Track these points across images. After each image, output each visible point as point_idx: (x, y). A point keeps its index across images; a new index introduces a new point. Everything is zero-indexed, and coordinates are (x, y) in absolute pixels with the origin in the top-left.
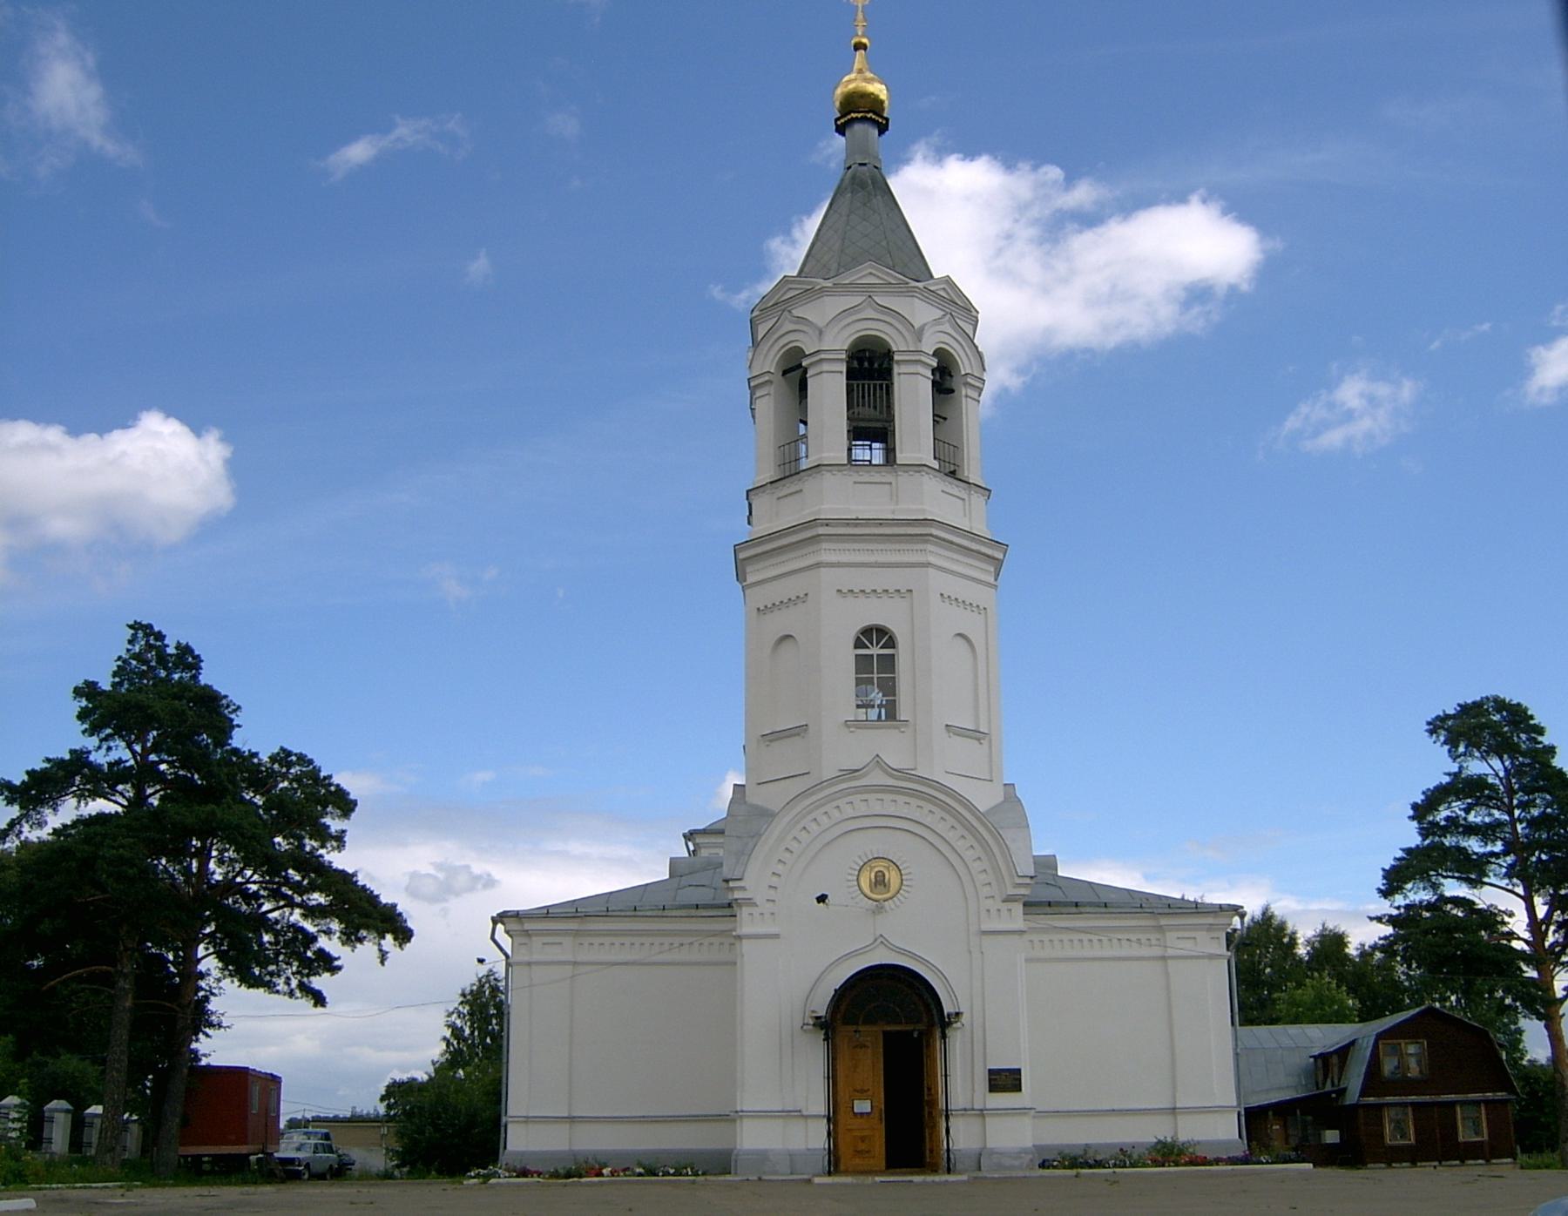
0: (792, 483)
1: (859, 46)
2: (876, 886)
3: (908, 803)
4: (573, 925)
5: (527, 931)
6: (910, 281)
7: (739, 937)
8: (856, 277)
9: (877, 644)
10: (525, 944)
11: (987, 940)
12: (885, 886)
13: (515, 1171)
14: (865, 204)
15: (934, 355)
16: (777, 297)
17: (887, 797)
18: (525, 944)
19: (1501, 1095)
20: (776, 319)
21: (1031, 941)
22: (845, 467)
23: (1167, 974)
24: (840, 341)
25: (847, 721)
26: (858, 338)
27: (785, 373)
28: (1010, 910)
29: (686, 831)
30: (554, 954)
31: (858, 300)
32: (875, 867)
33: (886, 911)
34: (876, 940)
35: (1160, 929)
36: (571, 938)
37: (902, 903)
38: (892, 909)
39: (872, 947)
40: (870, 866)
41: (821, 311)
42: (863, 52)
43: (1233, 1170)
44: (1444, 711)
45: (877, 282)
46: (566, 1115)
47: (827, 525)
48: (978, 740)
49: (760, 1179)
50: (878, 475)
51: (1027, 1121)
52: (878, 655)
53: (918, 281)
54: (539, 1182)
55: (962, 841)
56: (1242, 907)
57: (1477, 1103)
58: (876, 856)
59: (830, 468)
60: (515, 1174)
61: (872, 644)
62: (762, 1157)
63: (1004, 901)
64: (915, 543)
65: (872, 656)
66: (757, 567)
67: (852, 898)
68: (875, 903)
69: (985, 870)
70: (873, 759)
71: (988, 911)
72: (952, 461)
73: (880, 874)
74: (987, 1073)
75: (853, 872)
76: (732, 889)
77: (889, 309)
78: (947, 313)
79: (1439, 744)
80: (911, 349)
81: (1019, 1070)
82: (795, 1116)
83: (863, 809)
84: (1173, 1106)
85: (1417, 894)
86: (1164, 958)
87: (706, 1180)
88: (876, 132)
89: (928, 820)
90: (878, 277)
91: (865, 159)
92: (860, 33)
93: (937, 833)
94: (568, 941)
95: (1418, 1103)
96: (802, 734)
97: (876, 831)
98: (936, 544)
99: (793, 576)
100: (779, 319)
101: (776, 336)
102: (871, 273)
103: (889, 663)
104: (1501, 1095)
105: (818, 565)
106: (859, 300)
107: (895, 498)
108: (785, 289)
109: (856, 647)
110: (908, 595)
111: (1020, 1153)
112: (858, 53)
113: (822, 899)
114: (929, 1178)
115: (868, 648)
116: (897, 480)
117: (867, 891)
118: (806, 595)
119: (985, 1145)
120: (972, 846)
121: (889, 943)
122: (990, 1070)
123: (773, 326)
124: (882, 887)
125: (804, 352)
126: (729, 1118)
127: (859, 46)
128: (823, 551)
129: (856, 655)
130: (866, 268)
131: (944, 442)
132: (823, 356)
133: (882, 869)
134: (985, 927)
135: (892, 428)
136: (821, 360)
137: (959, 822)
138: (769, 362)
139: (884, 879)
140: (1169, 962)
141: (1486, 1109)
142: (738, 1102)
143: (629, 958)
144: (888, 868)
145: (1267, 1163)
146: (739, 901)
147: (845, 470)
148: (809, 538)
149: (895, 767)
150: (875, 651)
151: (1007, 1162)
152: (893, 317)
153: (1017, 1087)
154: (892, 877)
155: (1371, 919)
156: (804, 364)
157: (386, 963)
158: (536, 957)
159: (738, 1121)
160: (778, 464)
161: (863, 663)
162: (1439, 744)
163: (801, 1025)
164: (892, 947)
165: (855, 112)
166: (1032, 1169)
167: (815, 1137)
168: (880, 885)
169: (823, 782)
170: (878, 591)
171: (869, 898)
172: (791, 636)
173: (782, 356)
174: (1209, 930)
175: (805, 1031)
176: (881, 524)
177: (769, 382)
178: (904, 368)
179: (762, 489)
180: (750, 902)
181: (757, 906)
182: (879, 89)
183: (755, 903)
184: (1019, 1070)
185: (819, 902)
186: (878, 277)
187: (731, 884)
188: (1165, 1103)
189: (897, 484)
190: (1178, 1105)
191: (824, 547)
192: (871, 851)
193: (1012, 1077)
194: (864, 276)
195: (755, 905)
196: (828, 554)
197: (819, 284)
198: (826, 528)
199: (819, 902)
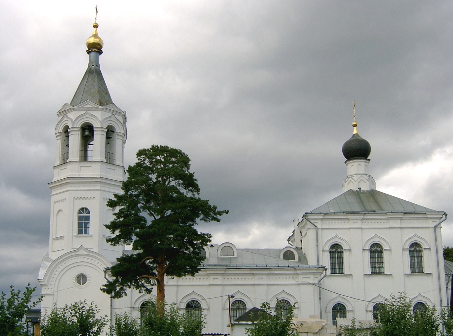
9: (85, 213)
15: (107, 128)
26: (83, 123)
41: (73, 115)
52: (85, 216)
61: (83, 213)
65: (83, 216)
72: (110, 158)
75: (74, 280)
76: (40, 282)
102: (88, 104)
103: (88, 218)
106: (84, 112)
109: (79, 213)
115: (82, 214)
118: (94, 197)
129: (79, 216)
131: (109, 153)
138: (61, 130)
148: (109, 184)
150: (84, 215)
156: (68, 131)
161: (80, 218)
172: (61, 210)
174: (267, 275)
187: (40, 281)
192: (75, 274)
194: (86, 105)
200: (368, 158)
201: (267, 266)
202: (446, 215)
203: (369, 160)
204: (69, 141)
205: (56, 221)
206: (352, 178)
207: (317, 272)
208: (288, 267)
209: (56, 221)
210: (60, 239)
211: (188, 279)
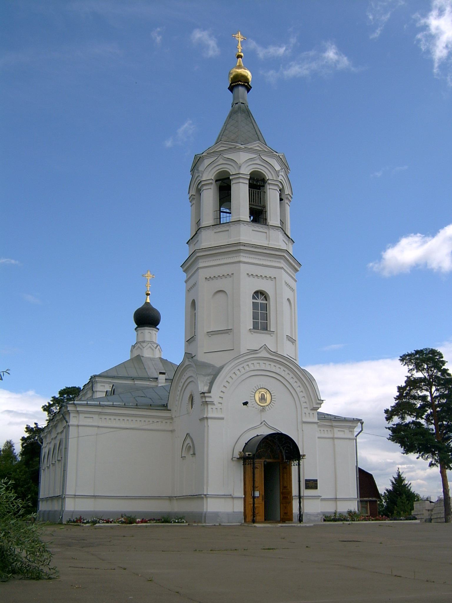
0: (223, 227)
1: (239, 56)
2: (261, 400)
3: (275, 366)
4: (99, 410)
5: (78, 411)
6: (274, 152)
7: (207, 418)
8: (254, 146)
10: (76, 417)
11: (305, 426)
12: (265, 400)
13: (105, 520)
14: (246, 119)
16: (216, 149)
17: (267, 363)
18: (76, 417)
19: (374, 499)
20: (217, 157)
22: (250, 223)
23: (334, 445)
24: (246, 171)
25: (250, 329)
27: (216, 181)
28: (313, 414)
29: (92, 375)
30: (89, 422)
31: (254, 156)
32: (261, 392)
33: (266, 411)
34: (261, 423)
35: (332, 426)
36: (97, 415)
37: (270, 409)
38: (268, 410)
39: (260, 426)
42: (241, 59)
43: (393, 522)
44: (408, 352)
45: (260, 149)
46: (93, 495)
47: (244, 246)
48: (293, 343)
49: (220, 525)
50: (257, 228)
51: (318, 502)
53: (277, 153)
54: (119, 525)
55: (296, 383)
56: (362, 420)
57: (366, 501)
58: (262, 387)
59: (244, 222)
60: (105, 522)
61: (258, 298)
62: (216, 515)
63: (311, 410)
64: (277, 258)
65: (258, 303)
66: (204, 260)
67: (252, 404)
68: (262, 407)
69: (304, 397)
71: (305, 413)
73: (263, 395)
74: (305, 481)
77: (267, 162)
78: (283, 168)
79: (403, 365)
80: (274, 179)
81: (317, 480)
82: (229, 497)
83: (257, 367)
84: (335, 497)
85: (396, 420)
86: (333, 438)
87: (343, 523)
88: (247, 92)
89: (283, 374)
90: (260, 147)
91: (243, 101)
92: (240, 51)
94: (96, 417)
95: (371, 501)
96: (229, 333)
98: (284, 261)
99: (228, 265)
101: (215, 165)
103: (265, 307)
104: (374, 499)
105: (239, 262)
107: (268, 239)
108: (220, 146)
110: (274, 280)
111: (317, 514)
112: (239, 59)
113: (245, 404)
114: (291, 525)
115: (257, 299)
116: (269, 231)
117: (258, 402)
118: (233, 274)
120: (299, 386)
121: (268, 424)
122: (306, 480)
123: (215, 160)
124: (264, 400)
125: (230, 174)
126: (200, 497)
127: (239, 56)
128: (241, 256)
130: (256, 143)
132: (241, 176)
133: (264, 393)
134: (304, 420)
135: (265, 211)
136: (239, 177)
137: (295, 376)
140: (336, 440)
141: (369, 504)
142: (205, 489)
143: (133, 426)
144: (266, 393)
145: (404, 520)
146: (208, 402)
147: (249, 224)
149: (273, 351)
150: (259, 301)
151: (313, 518)
152: (268, 165)
153: (316, 488)
154: (268, 396)
155: (386, 428)
156: (230, 178)
158: (81, 423)
159: (205, 499)
162: (403, 365)
163: (231, 458)
164: (268, 426)
165: (241, 82)
166: (322, 521)
167: (239, 507)
168: (263, 399)
169: (241, 355)
170: (263, 276)
171: (259, 405)
173: (219, 172)
174: (349, 428)
175: (233, 460)
176: (266, 248)
177: (211, 183)
178: (271, 187)
180: (212, 403)
181: (215, 405)
182: (248, 74)
183: (214, 404)
184: (317, 480)
185: (244, 405)
186: (260, 147)
188: (333, 496)
189: (269, 233)
190: (337, 497)
191: (241, 255)
192: (260, 385)
193: (314, 483)
195: (214, 404)
196: (243, 258)
197: (238, 146)
198: (244, 247)
199: (244, 405)
200: (157, 327)
201: (137, 405)
202: (362, 423)
203: (158, 329)
204: (200, 208)
205: (294, 296)
206: (141, 345)
207: (103, 411)
208: (99, 405)
209: (294, 296)
210: (226, 333)
211: (326, 432)
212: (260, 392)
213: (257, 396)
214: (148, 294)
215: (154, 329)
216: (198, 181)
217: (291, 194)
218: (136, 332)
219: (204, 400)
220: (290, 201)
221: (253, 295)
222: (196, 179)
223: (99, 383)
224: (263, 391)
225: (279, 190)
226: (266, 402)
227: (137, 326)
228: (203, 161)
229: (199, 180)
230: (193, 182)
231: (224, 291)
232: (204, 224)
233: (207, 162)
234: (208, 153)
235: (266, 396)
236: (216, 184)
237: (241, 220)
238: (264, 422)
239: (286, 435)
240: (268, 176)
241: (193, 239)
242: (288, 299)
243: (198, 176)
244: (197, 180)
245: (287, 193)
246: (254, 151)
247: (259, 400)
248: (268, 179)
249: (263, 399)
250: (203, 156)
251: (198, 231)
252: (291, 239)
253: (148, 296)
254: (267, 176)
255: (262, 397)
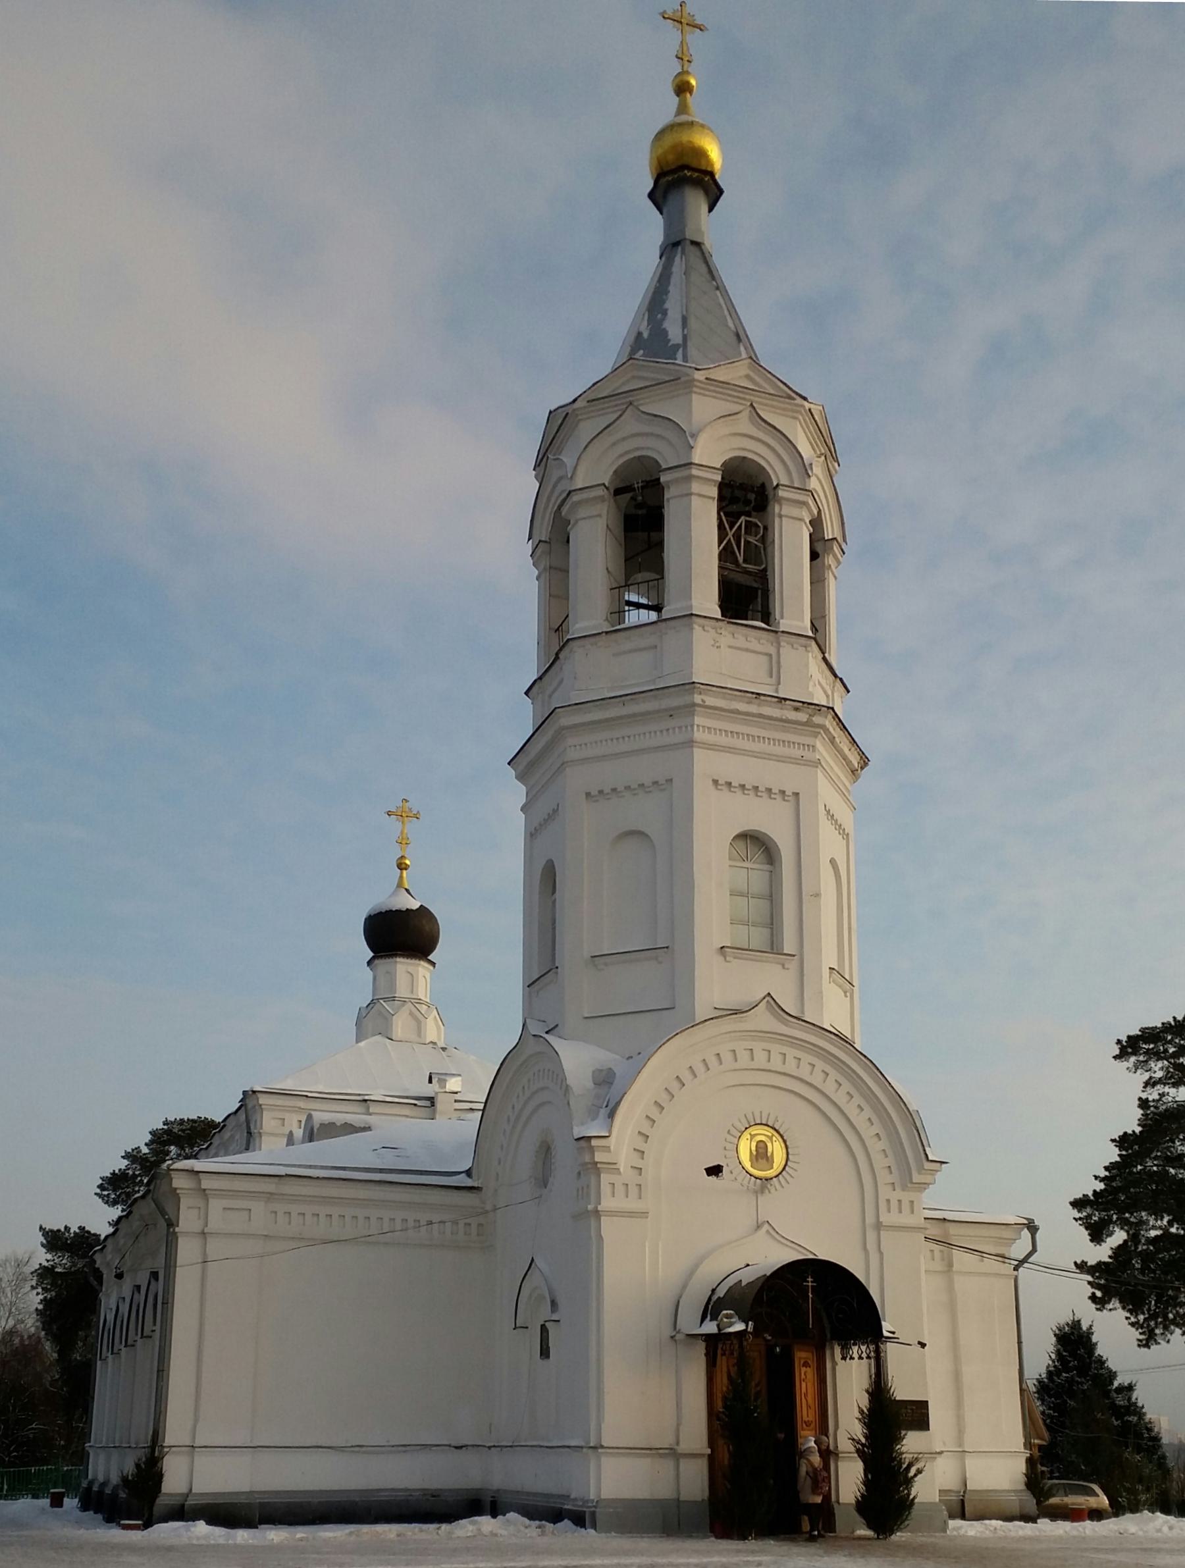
2: (757, 1160)
5: (204, 1190)
21: (932, 1251)
40: (750, 1134)
53: (805, 399)
70: (764, 998)
78: (822, 454)
80: (796, 485)
93: (397, 1183)
97: (758, 1087)
100: (621, 416)
117: (747, 1165)
119: (191, 1490)
139: (767, 1151)
144: (771, 1138)
154: (777, 1150)
157: (95, 1196)
160: (611, 611)
168: (762, 1158)
179: (592, 640)
184: (924, 1404)
200: (429, 958)
212: (752, 1136)
213: (745, 1149)
214: (403, 866)
215: (422, 963)
216: (560, 495)
217: (840, 539)
218: (371, 973)
219: (587, 1159)
220: (839, 563)
221: (101, 1284)
222: (555, 486)
223: (221, 1193)
224: (762, 1133)
225: (808, 522)
226: (772, 1168)
227: (372, 954)
228: (577, 426)
229: (563, 491)
230: (549, 489)
231: (647, 836)
232: (578, 627)
233: (587, 429)
234: (590, 399)
235: (770, 1150)
236: (615, 501)
237: (694, 612)
238: (766, 1226)
239: (841, 1267)
240: (778, 474)
241: (545, 679)
242: (833, 862)
243: (560, 479)
244: (556, 494)
245: (830, 537)
246: (736, 394)
247: (751, 1160)
248: (778, 485)
249: (761, 1154)
250: (574, 410)
251: (561, 649)
252: (841, 680)
253: (405, 872)
254: (773, 477)
255: (760, 1150)
